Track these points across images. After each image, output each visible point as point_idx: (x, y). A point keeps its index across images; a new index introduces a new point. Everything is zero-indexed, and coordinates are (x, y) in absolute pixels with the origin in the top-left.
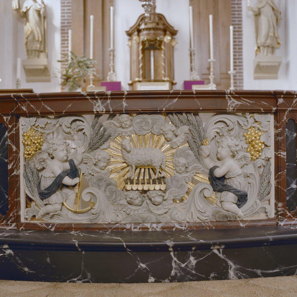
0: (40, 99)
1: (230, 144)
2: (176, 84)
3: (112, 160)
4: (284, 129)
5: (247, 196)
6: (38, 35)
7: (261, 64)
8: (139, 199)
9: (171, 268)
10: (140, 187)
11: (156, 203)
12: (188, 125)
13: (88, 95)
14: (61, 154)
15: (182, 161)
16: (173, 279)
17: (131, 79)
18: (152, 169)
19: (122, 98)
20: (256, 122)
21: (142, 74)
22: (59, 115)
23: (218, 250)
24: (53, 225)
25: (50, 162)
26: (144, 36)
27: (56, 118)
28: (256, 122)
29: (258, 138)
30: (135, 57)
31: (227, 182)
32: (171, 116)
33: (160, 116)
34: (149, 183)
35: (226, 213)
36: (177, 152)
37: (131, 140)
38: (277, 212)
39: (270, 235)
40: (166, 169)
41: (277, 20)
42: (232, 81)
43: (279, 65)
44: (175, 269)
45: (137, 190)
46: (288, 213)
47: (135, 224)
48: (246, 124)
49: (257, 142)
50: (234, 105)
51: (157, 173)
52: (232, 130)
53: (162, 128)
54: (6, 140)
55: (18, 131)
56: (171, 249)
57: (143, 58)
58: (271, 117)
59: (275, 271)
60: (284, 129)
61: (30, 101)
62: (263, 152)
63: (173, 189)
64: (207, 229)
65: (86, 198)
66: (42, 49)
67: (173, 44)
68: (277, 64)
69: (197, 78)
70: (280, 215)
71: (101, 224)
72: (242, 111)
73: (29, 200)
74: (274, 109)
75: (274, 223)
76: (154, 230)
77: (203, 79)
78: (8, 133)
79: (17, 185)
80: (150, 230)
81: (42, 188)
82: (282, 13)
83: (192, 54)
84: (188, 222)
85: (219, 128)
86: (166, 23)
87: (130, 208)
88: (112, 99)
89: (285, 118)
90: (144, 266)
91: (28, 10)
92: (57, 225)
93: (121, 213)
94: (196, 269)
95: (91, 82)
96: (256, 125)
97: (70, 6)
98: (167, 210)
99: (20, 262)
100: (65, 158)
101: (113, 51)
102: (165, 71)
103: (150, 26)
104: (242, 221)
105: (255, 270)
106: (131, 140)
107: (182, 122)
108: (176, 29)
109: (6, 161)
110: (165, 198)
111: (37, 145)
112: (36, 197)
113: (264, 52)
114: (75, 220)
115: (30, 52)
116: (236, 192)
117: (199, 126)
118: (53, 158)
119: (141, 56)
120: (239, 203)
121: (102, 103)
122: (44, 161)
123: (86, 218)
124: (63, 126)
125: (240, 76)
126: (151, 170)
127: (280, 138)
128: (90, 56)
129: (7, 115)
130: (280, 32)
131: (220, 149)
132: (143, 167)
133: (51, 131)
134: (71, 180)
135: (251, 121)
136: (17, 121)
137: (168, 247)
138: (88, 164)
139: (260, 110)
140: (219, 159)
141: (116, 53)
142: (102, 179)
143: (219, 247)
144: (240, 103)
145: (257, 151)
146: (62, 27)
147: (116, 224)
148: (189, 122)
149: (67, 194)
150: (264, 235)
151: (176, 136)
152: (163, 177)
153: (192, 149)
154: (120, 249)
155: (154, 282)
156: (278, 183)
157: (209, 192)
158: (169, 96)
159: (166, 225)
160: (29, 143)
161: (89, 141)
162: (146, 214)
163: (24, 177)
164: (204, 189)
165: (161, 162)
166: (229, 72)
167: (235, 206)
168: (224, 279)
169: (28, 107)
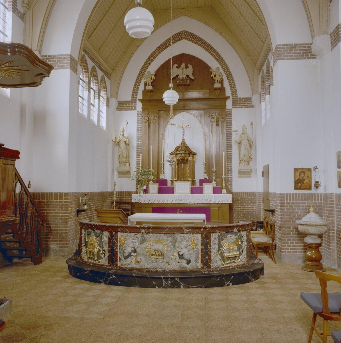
7: (241, 170)
9: (163, 284)
15: (169, 249)
16: (163, 287)
23: (177, 279)
26: (178, 157)
31: (184, 256)
34: (158, 256)
35: (183, 266)
43: (251, 171)
55: (117, 237)
58: (200, 235)
59: (196, 286)
67: (194, 160)
68: (250, 170)
73: (120, 259)
81: (125, 256)
90: (155, 283)
103: (181, 152)
112: (123, 258)
113: (243, 164)
116: (186, 260)
129: (114, 232)
136: (117, 234)
148: (171, 237)
149: (132, 258)
151: (167, 241)
156: (202, 257)
157: (178, 259)
162: (157, 266)
169: (121, 229)
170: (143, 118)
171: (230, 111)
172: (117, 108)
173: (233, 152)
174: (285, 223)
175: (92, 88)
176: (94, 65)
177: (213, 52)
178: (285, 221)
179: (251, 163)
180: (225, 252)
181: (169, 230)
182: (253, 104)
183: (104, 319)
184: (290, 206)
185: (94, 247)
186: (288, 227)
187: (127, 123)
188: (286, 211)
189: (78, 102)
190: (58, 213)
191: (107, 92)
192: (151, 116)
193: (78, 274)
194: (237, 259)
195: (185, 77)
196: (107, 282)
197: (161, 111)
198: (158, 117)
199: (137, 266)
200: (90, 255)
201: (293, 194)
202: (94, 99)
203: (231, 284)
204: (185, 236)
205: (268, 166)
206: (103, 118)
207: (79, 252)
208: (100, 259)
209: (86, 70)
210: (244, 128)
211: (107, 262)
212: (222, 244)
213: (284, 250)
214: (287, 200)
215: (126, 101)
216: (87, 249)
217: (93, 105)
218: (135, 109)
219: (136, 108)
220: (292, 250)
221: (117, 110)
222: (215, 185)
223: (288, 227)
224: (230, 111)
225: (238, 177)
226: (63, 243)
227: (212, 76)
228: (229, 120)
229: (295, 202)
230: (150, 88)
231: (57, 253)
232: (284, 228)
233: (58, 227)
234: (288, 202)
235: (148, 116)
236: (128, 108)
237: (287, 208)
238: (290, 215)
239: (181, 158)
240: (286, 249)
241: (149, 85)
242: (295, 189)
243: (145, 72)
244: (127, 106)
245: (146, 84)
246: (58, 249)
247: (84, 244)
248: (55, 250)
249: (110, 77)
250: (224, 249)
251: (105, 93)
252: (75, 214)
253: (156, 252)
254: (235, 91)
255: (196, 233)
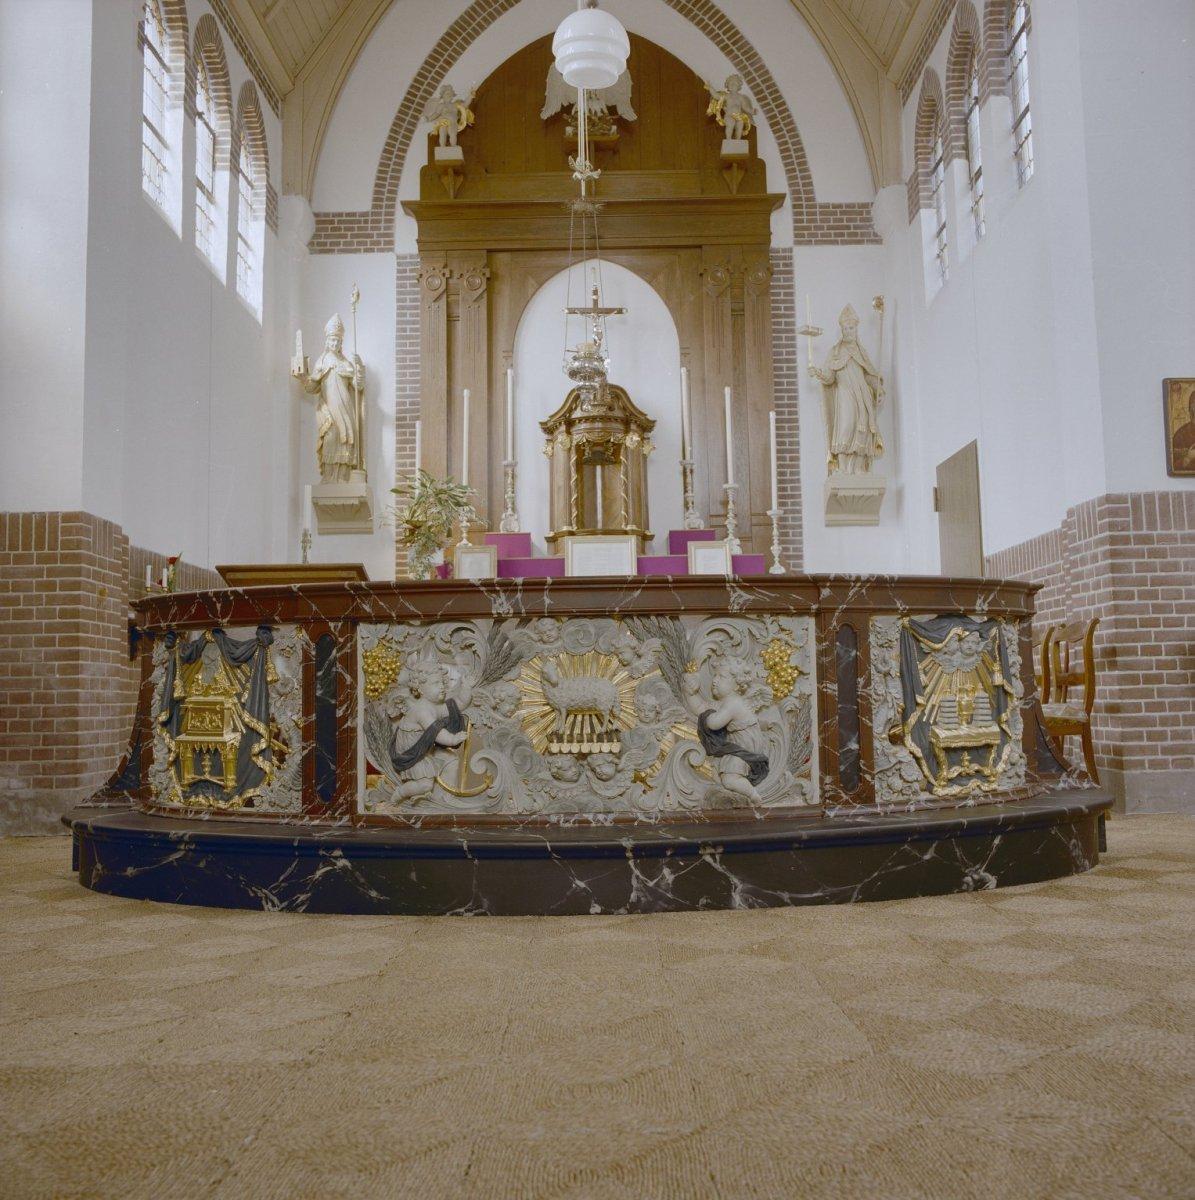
0: (396, 591)
1: (735, 671)
2: (652, 537)
3: (525, 699)
4: (832, 643)
5: (767, 763)
6: (346, 429)
7: (841, 493)
8: (574, 769)
10: (575, 747)
11: (604, 777)
12: (660, 637)
13: (483, 585)
14: (434, 690)
15: (650, 700)
17: (552, 528)
18: (596, 715)
19: (543, 590)
20: (783, 630)
21: (577, 516)
22: (430, 619)
23: (713, 855)
24: (418, 817)
25: (412, 703)
26: (580, 433)
27: (423, 624)
28: (783, 630)
29: (786, 659)
30: (560, 480)
31: (732, 739)
32: (629, 621)
33: (611, 620)
34: (590, 740)
36: (640, 685)
37: (559, 664)
38: (824, 792)
39: (803, 829)
40: (622, 715)
41: (875, 396)
42: (775, 532)
43: (881, 495)
44: (637, 890)
45: (570, 753)
46: (843, 795)
47: (566, 814)
48: (765, 634)
49: (784, 666)
50: (741, 601)
51: (606, 722)
52: (739, 645)
53: (614, 642)
54: (333, 664)
56: (629, 854)
57: (580, 481)
58: (810, 623)
59: (815, 895)
60: (832, 643)
61: (377, 595)
62: (797, 685)
63: (634, 751)
64: (694, 824)
65: (478, 768)
66: (355, 462)
68: (876, 493)
69: (700, 524)
70: (833, 799)
71: (504, 816)
72: (757, 610)
74: (814, 607)
75: (818, 812)
76: (599, 825)
77: (711, 526)
78: (338, 652)
79: (353, 747)
80: (593, 825)
82: (885, 382)
83: (688, 471)
84: (661, 811)
85: (716, 642)
86: (629, 405)
87: (557, 787)
88: (525, 591)
89: (835, 623)
90: (582, 884)
91: (324, 377)
92: (426, 817)
93: (542, 796)
94: (674, 891)
95: (465, 535)
96: (782, 635)
97: (416, 367)
98: (623, 790)
99: (362, 880)
100: (441, 697)
101: (513, 466)
102: (627, 512)
104: (759, 809)
105: (779, 892)
106: (559, 664)
107: (650, 632)
108: (650, 417)
109: (333, 702)
110: (620, 767)
111: (390, 673)
112: (388, 769)
113: (846, 465)
114: (457, 809)
115: (327, 468)
116: (745, 755)
117: (680, 638)
118: (418, 697)
119: (574, 476)
120: (752, 776)
121: (508, 599)
122: (402, 701)
123: (477, 805)
124: (438, 640)
125: (794, 519)
126: (594, 716)
127: (825, 660)
128: (461, 478)
130: (882, 424)
131: (717, 680)
132: (581, 712)
133: (415, 648)
134: (452, 735)
135: (774, 628)
136: (354, 630)
137: (624, 849)
138: (482, 707)
139: (789, 609)
140: (716, 698)
141: (518, 470)
142: (508, 734)
143: (713, 851)
144: (752, 597)
145: (785, 682)
146: (398, 412)
147: (531, 814)
148: (662, 633)
150: (794, 830)
151: (639, 656)
152: (617, 730)
153: (667, 680)
154: (538, 853)
155: (600, 914)
156: (824, 741)
157: (699, 757)
158: (625, 586)
159: (622, 816)
160: (376, 669)
161: (482, 667)
163: (365, 732)
164: (690, 751)
165: (612, 703)
166: (769, 513)
167: (746, 782)
168: (724, 908)
169: (375, 605)
170: (423, 281)
171: (787, 257)
172: (311, 244)
173: (802, 423)
174: (1133, 630)
175: (200, 115)
176: (213, 13)
177: (715, 24)
178: (1135, 620)
179: (875, 465)
180: (935, 723)
181: (646, 592)
182: (877, 229)
183: (309, 1065)
184: (1153, 553)
185: (222, 720)
186: (1146, 651)
187: (358, 296)
188: (1134, 574)
189: (139, 143)
190: (28, 614)
191: (267, 160)
192: (456, 275)
193: (130, 871)
194: (991, 762)
195: (602, 111)
196: (302, 897)
197: (501, 256)
198: (488, 279)
199: (468, 805)
200: (199, 770)
201: (1164, 497)
202: (214, 170)
203: (992, 881)
204: (737, 626)
205: (970, 454)
206: (249, 272)
207: (131, 777)
208: (256, 785)
209: (172, 12)
210: (848, 317)
211: (296, 797)
212: (923, 678)
213: (1132, 758)
214: (1138, 525)
215: (348, 215)
216: (183, 737)
217: (210, 196)
218: (389, 245)
219: (391, 243)
220: (1173, 755)
221: (313, 252)
222: (738, 551)
223: (1146, 651)
224: (785, 258)
225: (827, 526)
226: (55, 761)
227: (709, 111)
228: (782, 291)
229: (1173, 531)
230: (453, 153)
231: (20, 814)
232: (1132, 652)
233: (29, 684)
234: (1145, 532)
235: (444, 275)
236: (359, 243)
237: (1141, 560)
238: (1153, 595)
239: (593, 437)
240: (1142, 750)
241: (448, 143)
242: (1171, 474)
243: (435, 88)
244: (353, 236)
245: (433, 141)
246: (31, 793)
247: (163, 717)
248: (15, 798)
249: (280, 105)
250: (933, 706)
251: (259, 166)
252: (122, 736)
253: (578, 724)
254: (803, 178)
255: (792, 615)
